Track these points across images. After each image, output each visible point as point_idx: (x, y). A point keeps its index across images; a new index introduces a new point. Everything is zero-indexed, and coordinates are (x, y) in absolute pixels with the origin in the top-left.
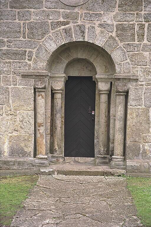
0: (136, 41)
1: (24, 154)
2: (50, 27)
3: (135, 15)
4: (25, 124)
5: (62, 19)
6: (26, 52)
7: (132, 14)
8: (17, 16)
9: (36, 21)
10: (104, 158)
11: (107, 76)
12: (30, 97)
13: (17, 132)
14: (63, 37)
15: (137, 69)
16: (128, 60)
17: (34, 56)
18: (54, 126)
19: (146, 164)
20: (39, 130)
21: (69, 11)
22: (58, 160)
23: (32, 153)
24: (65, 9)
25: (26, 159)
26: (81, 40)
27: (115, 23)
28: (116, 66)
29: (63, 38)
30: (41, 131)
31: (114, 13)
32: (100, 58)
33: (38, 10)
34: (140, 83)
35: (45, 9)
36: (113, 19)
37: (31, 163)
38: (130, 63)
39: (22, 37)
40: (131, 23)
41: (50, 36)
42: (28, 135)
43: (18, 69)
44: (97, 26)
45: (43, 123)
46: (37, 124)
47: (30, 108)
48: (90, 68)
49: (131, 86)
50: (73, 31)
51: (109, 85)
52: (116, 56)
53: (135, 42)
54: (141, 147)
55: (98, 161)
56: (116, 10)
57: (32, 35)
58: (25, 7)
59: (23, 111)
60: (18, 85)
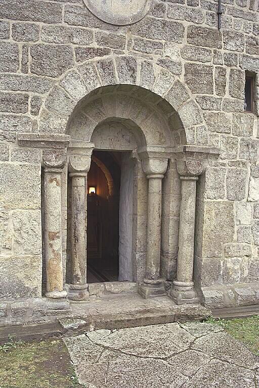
0: (215, 93)
1: (24, 292)
2: (75, 56)
3: (213, 53)
4: (25, 235)
5: (95, 45)
6: (27, 97)
7: (208, 51)
8: (11, 31)
9: (48, 44)
10: (158, 284)
11: (164, 149)
12: (35, 184)
13: (9, 252)
14: (99, 75)
15: (217, 139)
16: (204, 124)
17: (43, 107)
18: (73, 235)
19: (231, 291)
20: (51, 245)
21: (108, 32)
22: (82, 295)
23: (40, 290)
24: (100, 29)
25: (30, 303)
26: (129, 83)
27: (184, 62)
28: (187, 131)
29: (97, 78)
30: (56, 248)
31: (182, 46)
32: (151, 119)
33: (52, 25)
34: (221, 161)
35: (64, 24)
36: (180, 54)
37: (39, 311)
38: (206, 127)
39: (19, 71)
40: (206, 64)
41: (73, 71)
42: (32, 256)
43: (11, 129)
44: (156, 62)
45: (58, 232)
46: (47, 234)
47: (35, 205)
48: (128, 138)
49: (208, 166)
50: (116, 67)
51: (165, 164)
52: (186, 114)
53: (213, 95)
54: (222, 264)
55: (148, 290)
56: (185, 41)
57: (39, 67)
58: (27, 18)
59: (20, 210)
60: (12, 161)
